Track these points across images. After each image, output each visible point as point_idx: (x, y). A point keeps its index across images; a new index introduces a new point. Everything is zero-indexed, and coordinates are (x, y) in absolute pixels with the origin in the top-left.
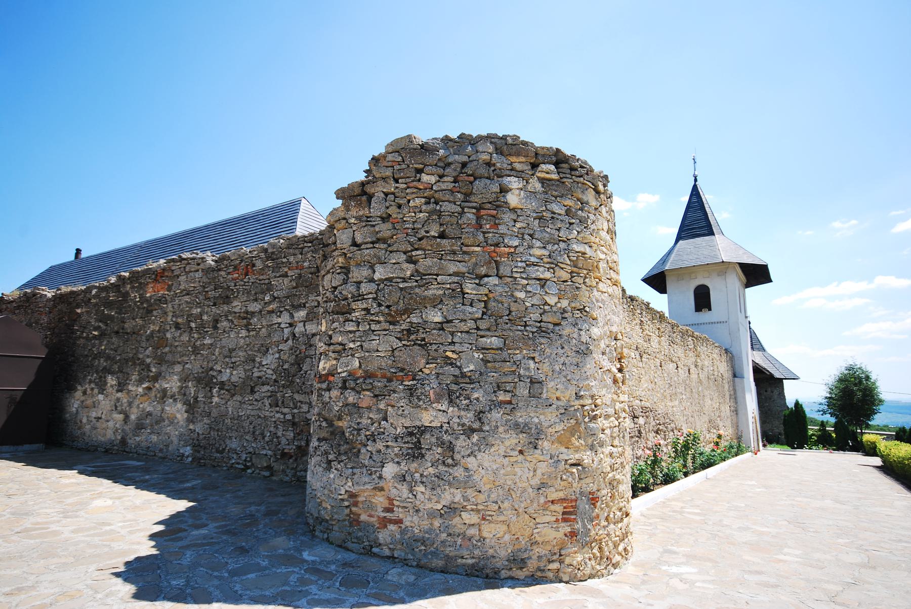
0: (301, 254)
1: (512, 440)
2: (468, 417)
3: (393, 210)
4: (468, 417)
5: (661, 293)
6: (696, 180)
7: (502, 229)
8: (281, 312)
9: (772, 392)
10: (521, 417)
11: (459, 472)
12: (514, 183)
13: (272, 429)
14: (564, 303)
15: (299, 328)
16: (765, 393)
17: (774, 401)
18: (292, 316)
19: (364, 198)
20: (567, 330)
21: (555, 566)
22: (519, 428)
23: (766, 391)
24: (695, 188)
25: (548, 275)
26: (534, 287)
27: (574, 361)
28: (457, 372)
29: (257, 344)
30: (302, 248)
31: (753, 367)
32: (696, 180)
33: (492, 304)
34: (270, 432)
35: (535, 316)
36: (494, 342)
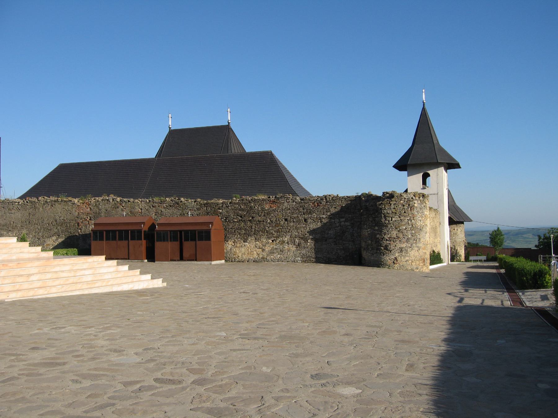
0: (341, 202)
1: (416, 249)
2: (410, 245)
3: (396, 207)
4: (410, 245)
5: (400, 171)
6: (424, 105)
7: (414, 211)
8: (335, 219)
9: (457, 230)
10: (418, 245)
11: (408, 254)
12: (416, 202)
13: (335, 251)
14: (423, 224)
15: (343, 223)
16: (453, 230)
17: (458, 235)
18: (339, 220)
19: (390, 204)
20: (424, 229)
21: (422, 269)
22: (418, 247)
23: (454, 230)
24: (424, 109)
25: (421, 219)
26: (419, 222)
27: (425, 235)
28: (408, 237)
29: (139, 200)
30: (342, 201)
31: (449, 217)
32: (424, 105)
33: (413, 225)
34: (335, 252)
35: (419, 227)
36: (414, 232)
